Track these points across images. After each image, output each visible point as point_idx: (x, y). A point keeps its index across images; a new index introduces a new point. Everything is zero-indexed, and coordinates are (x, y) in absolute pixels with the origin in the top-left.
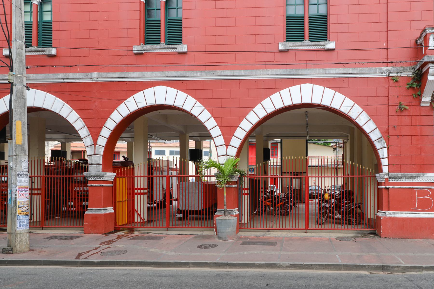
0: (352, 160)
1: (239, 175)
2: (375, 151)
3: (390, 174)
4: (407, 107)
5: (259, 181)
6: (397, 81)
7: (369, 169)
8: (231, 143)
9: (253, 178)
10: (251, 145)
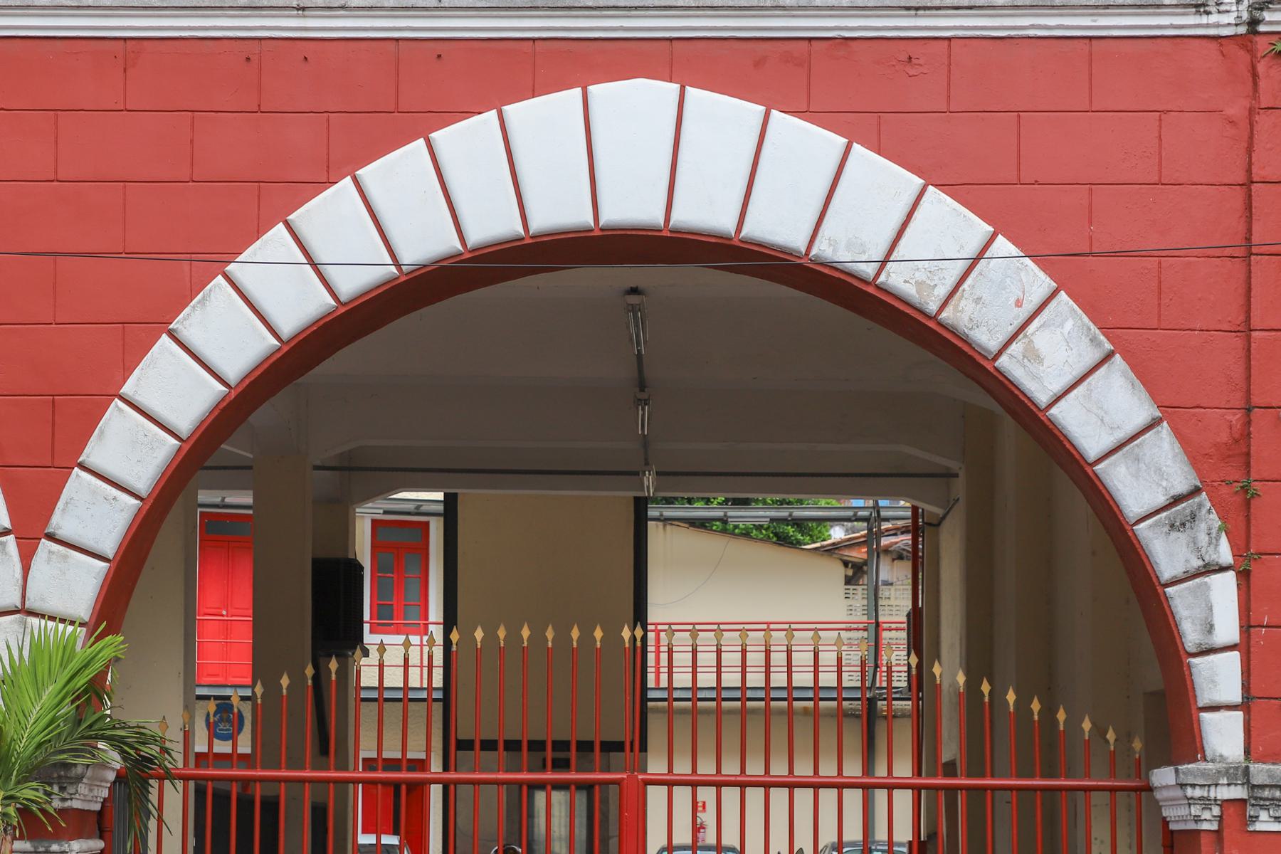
0: (979, 660)
1: (115, 759)
2: (1145, 592)
3: (1255, 768)
5: (271, 807)
7: (1100, 731)
8: (63, 521)
9: (222, 786)
10: (221, 532)
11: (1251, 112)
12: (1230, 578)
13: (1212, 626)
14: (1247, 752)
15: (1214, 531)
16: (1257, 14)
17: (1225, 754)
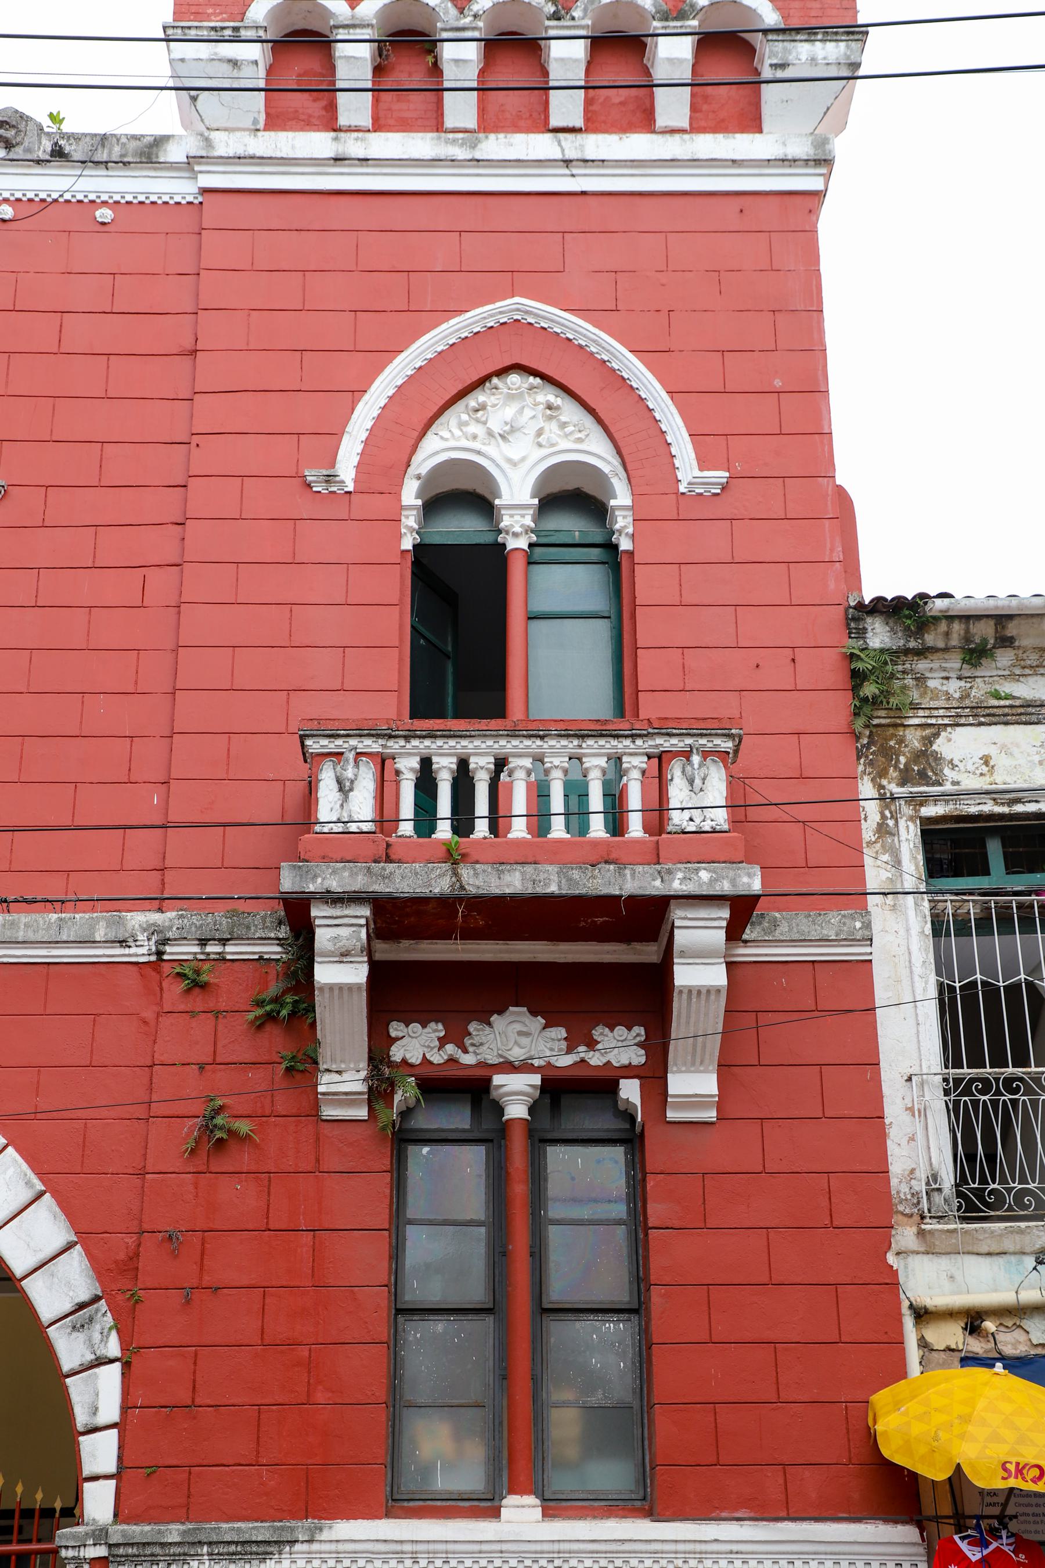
4: (243, 1127)
6: (204, 986)
11: (158, 1015)
12: (116, 1368)
13: (97, 1409)
14: (116, 1515)
15: (106, 1331)
16: (161, 948)
17: (97, 1518)
